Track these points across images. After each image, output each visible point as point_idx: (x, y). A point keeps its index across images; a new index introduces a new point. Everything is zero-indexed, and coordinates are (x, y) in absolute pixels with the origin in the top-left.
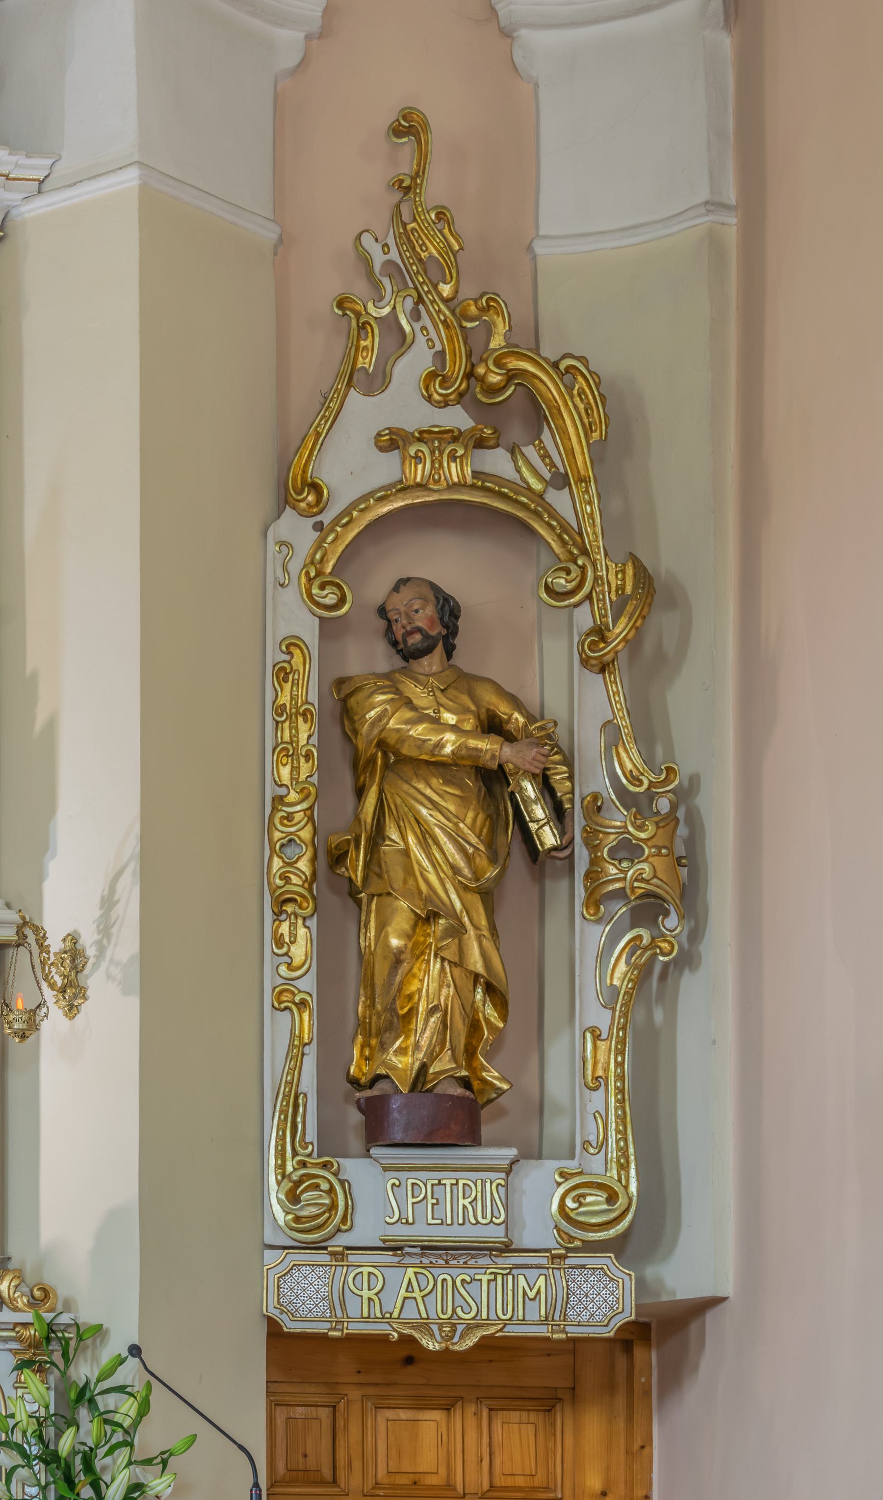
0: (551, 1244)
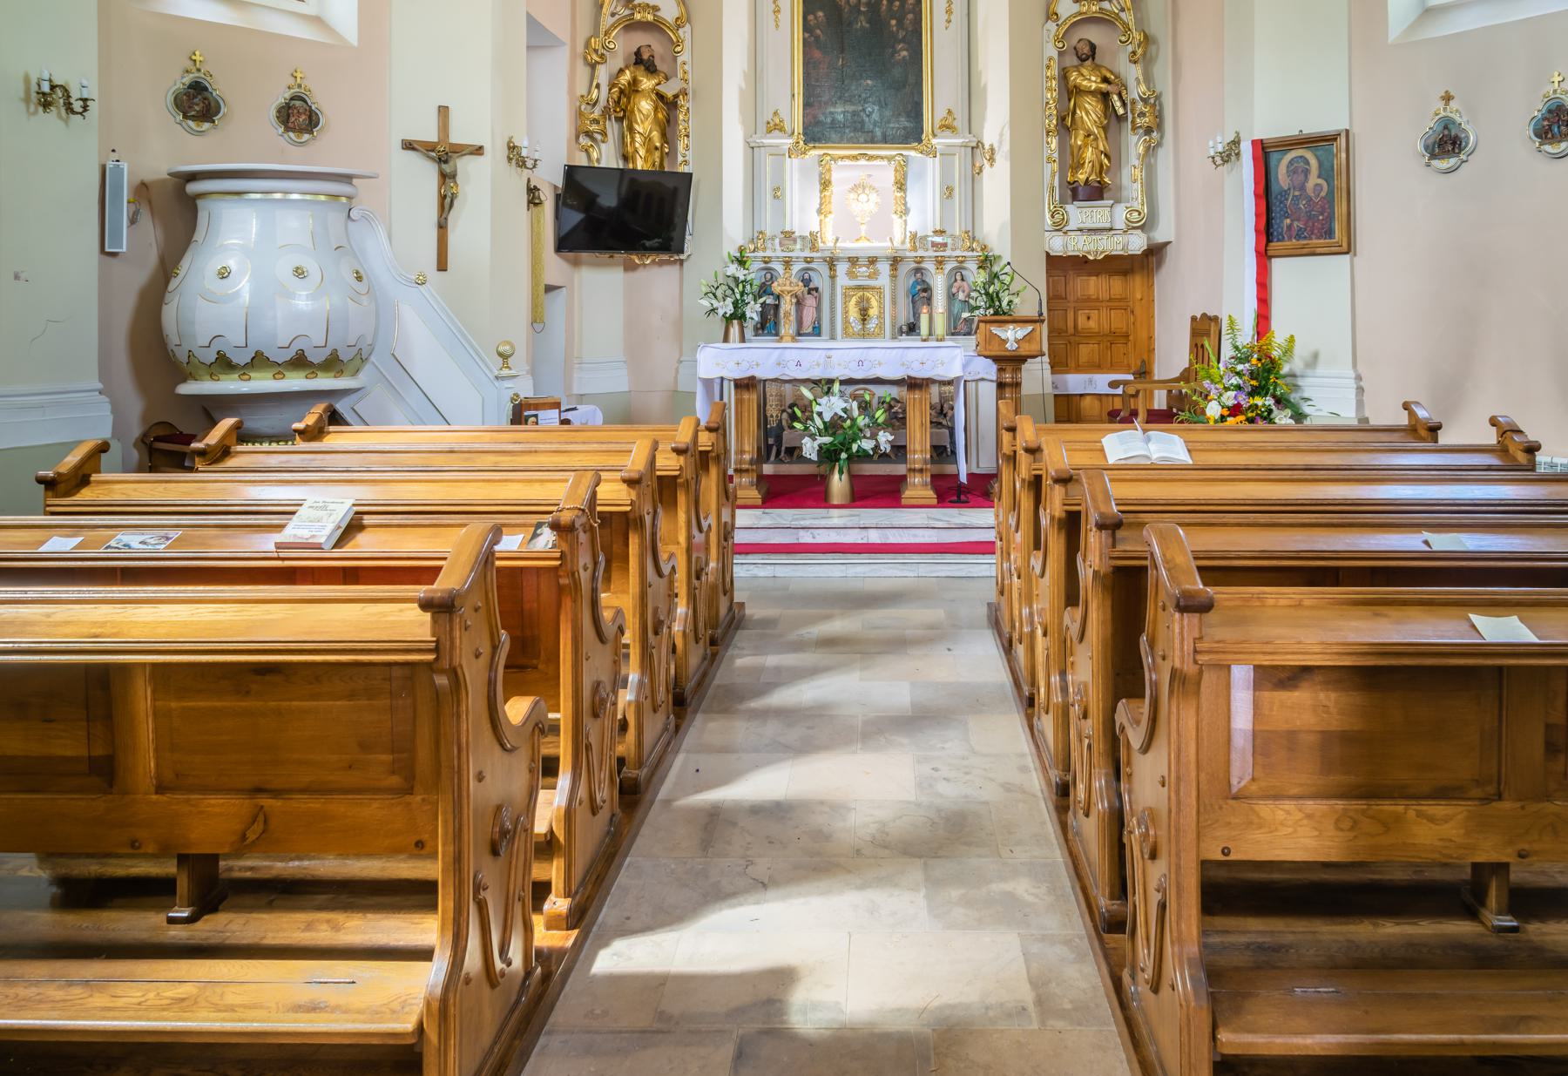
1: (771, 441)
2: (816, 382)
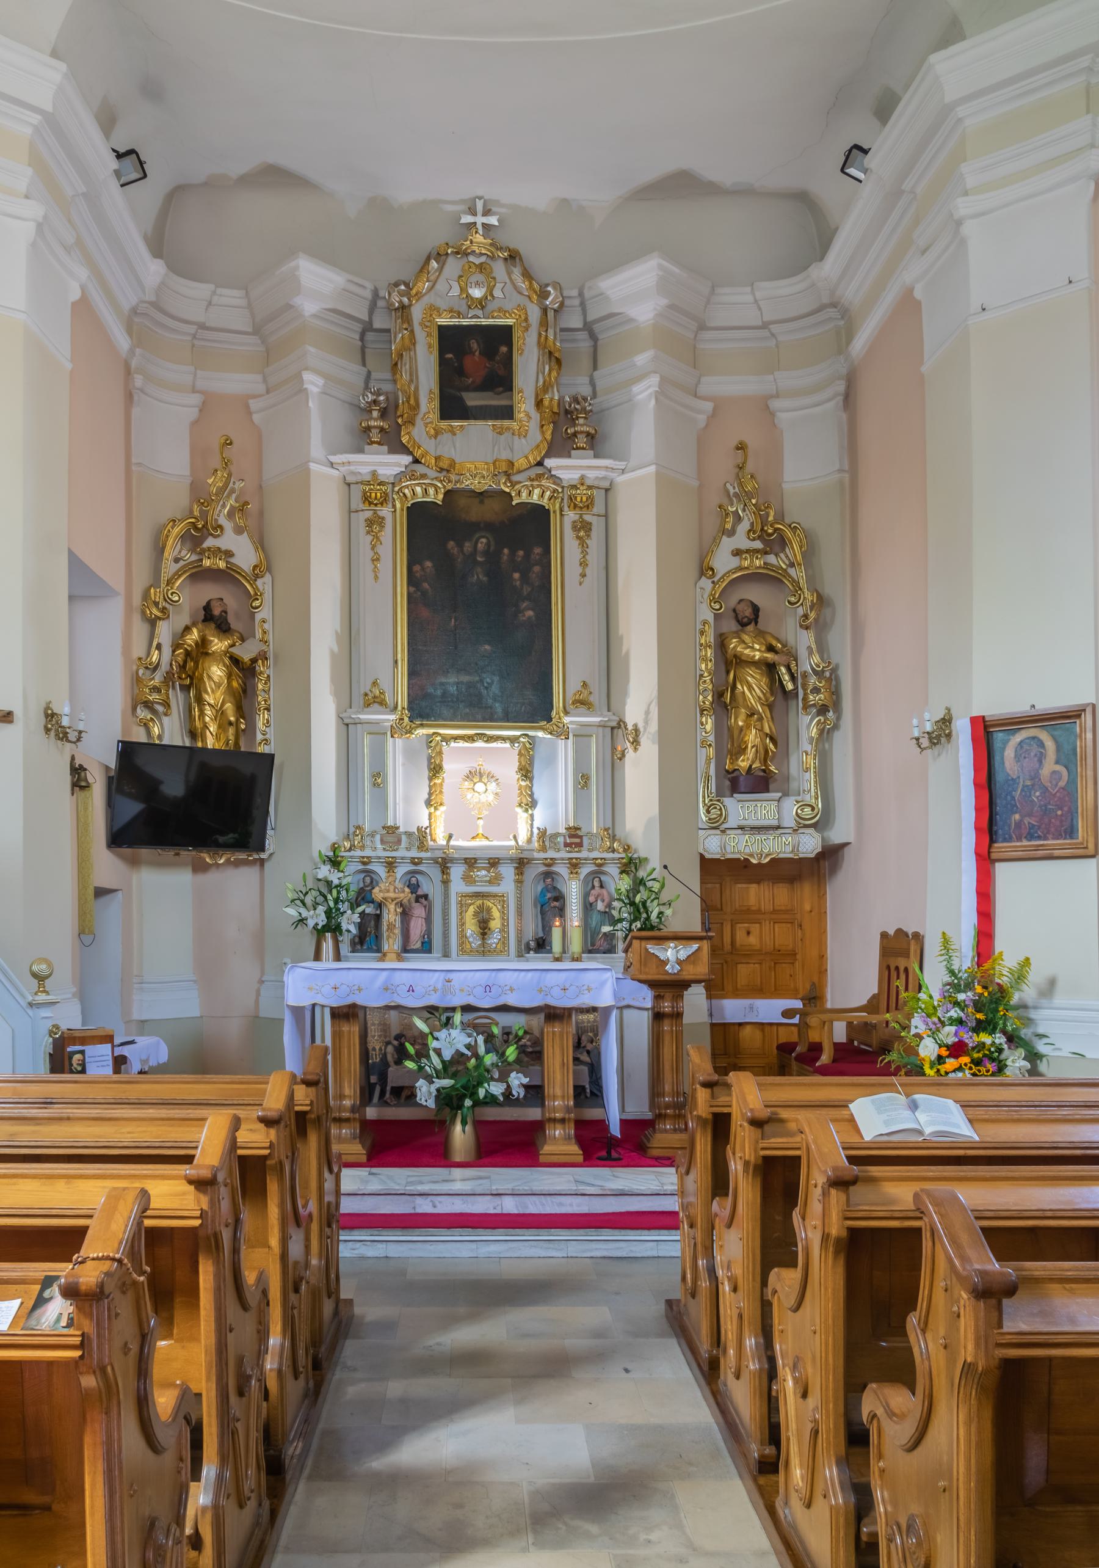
1: (373, 1079)
2: (432, 1010)
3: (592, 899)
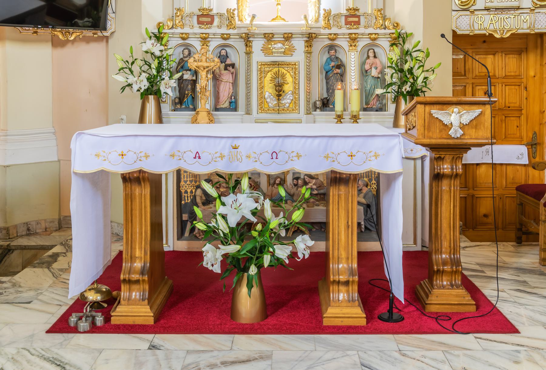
0: (531, 6)
3: (367, 67)
